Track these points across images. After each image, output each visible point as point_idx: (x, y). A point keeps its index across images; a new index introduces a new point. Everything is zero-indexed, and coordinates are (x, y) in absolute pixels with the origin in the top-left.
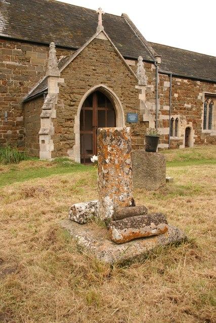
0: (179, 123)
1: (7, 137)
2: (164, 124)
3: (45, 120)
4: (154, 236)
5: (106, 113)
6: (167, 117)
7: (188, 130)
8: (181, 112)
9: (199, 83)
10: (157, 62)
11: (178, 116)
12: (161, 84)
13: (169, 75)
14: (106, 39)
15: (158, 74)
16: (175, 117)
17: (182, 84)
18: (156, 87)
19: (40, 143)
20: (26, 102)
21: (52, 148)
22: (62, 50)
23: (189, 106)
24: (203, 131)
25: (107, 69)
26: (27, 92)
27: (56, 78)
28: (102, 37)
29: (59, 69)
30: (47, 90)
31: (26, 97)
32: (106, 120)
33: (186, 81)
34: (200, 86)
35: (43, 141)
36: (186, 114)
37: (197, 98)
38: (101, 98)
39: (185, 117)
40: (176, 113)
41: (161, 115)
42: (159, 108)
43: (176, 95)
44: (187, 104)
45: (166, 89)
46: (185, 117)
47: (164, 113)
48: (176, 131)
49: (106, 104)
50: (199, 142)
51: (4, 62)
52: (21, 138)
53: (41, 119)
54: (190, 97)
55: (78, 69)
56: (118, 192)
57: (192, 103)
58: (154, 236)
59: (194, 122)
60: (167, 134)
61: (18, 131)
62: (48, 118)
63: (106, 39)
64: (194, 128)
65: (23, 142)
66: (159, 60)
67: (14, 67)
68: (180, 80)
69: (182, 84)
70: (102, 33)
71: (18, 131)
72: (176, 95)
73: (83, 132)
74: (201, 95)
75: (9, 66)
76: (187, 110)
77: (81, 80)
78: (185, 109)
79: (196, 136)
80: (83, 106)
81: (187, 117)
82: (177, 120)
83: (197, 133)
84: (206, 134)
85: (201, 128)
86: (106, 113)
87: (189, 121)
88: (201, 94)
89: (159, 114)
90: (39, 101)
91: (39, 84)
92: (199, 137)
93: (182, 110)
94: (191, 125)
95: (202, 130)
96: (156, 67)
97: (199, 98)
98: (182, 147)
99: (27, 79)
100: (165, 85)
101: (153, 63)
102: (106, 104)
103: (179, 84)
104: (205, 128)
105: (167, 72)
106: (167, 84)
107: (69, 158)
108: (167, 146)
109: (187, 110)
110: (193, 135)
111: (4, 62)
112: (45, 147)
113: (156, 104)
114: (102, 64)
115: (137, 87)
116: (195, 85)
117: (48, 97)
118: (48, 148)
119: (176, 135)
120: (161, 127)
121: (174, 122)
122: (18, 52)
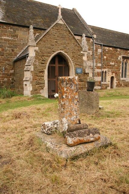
0: (107, 74)
1: (4, 82)
2: (98, 74)
3: (27, 72)
4: (92, 142)
6: (100, 71)
7: (112, 78)
8: (108, 68)
9: (119, 50)
10: (94, 38)
11: (107, 70)
12: (96, 50)
13: (101, 45)
14: (63, 24)
15: (94, 45)
16: (104, 70)
17: (109, 50)
18: (93, 52)
19: (24, 86)
20: (16, 61)
21: (31, 89)
22: (37, 30)
23: (113, 64)
24: (121, 79)
25: (64, 41)
26: (16, 55)
27: (34, 47)
28: (61, 22)
29: (35, 42)
30: (28, 54)
31: (15, 58)
32: (63, 72)
33: (111, 49)
34: (119, 52)
35: (26, 85)
36: (111, 69)
37: (117, 59)
38: (60, 59)
39: (110, 70)
40: (105, 68)
41: (96, 69)
42: (95, 65)
43: (105, 57)
44: (112, 62)
45: (99, 54)
46: (110, 70)
47: (98, 68)
48: (105, 79)
49: (63, 62)
50: (119, 85)
51: (2, 37)
52: (13, 83)
53: (25, 72)
54: (114, 58)
55: (46, 42)
56: (71, 115)
57: (115, 62)
58: (92, 142)
59: (116, 74)
60: (100, 80)
61: (11, 79)
62: (29, 71)
63: (63, 24)
64: (116, 77)
65: (14, 85)
66: (95, 36)
67: (9, 40)
68: (107, 48)
69: (109, 50)
70: (61, 20)
71: (11, 79)
72: (105, 57)
73: (49, 79)
74: (120, 57)
75: (5, 40)
76: (112, 66)
77: (48, 48)
78: (110, 65)
79: (117, 82)
80: (49, 64)
81: (112, 70)
82: (106, 72)
83: (118, 80)
84: (123, 80)
85: (120, 77)
87: (113, 73)
88: (120, 57)
89: (95, 69)
90: (24, 61)
91: (23, 51)
92: (119, 82)
93: (109, 66)
94: (114, 75)
95: (121, 78)
96: (93, 40)
97: (119, 59)
98: (109, 88)
99: (16, 48)
100: (98, 51)
101: (91, 38)
102: (63, 62)
103: (107, 50)
104: (122, 77)
105: (100, 43)
106: (100, 51)
108: (100, 87)
109: (112, 66)
110: (115, 81)
111: (2, 37)
112: (27, 88)
113: (93, 62)
114: (61, 38)
115: (82, 52)
116: (117, 51)
117: (29, 58)
118: (28, 89)
119: (105, 81)
120: (96, 76)
121: (104, 73)
122: (11, 31)
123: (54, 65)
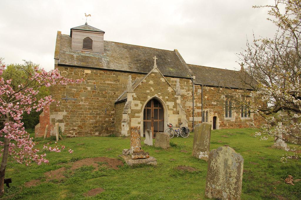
0: (209, 114)
1: (105, 122)
2: (198, 114)
3: (125, 114)
4: (144, 158)
6: (200, 111)
7: (215, 118)
8: (209, 107)
10: (193, 79)
11: (208, 110)
12: (196, 91)
13: (201, 85)
14: (158, 72)
15: (194, 85)
16: (206, 110)
17: (210, 90)
18: (192, 93)
19: (122, 126)
20: (117, 103)
21: (128, 129)
23: (215, 103)
24: (225, 119)
25: (158, 87)
26: (117, 98)
27: (132, 93)
28: (156, 71)
29: (133, 89)
30: (127, 99)
31: (116, 101)
32: (158, 114)
33: (212, 88)
35: (123, 125)
37: (220, 98)
38: (156, 102)
39: (212, 110)
40: (206, 108)
41: (196, 110)
43: (206, 97)
45: (199, 94)
46: (212, 110)
47: (198, 108)
48: (207, 119)
49: (158, 105)
50: (223, 125)
51: (106, 82)
52: (113, 122)
53: (123, 114)
55: (143, 88)
56: (135, 145)
58: (144, 158)
59: (219, 113)
60: (200, 121)
61: (111, 119)
62: (126, 113)
63: (158, 72)
65: (114, 125)
66: (194, 77)
67: (111, 84)
69: (210, 90)
70: (156, 69)
71: (111, 119)
72: (206, 97)
73: (146, 121)
75: (108, 84)
76: (214, 106)
77: (144, 94)
78: (212, 105)
79: (221, 122)
80: (145, 107)
81: (214, 110)
82: (207, 112)
83: (221, 120)
84: (227, 120)
85: (224, 117)
90: (123, 104)
91: (124, 93)
92: (223, 122)
95: (225, 118)
96: (193, 81)
99: (117, 91)
100: (198, 92)
101: (191, 79)
102: (158, 105)
103: (208, 90)
104: (226, 116)
105: (200, 84)
106: (200, 91)
109: (214, 106)
110: (218, 121)
111: (106, 82)
112: (124, 129)
113: (193, 102)
114: (156, 85)
115: (175, 96)
117: (127, 102)
118: (126, 128)
119: (207, 121)
120: (196, 116)
121: (205, 114)
122: (113, 77)
123: (51, 120)
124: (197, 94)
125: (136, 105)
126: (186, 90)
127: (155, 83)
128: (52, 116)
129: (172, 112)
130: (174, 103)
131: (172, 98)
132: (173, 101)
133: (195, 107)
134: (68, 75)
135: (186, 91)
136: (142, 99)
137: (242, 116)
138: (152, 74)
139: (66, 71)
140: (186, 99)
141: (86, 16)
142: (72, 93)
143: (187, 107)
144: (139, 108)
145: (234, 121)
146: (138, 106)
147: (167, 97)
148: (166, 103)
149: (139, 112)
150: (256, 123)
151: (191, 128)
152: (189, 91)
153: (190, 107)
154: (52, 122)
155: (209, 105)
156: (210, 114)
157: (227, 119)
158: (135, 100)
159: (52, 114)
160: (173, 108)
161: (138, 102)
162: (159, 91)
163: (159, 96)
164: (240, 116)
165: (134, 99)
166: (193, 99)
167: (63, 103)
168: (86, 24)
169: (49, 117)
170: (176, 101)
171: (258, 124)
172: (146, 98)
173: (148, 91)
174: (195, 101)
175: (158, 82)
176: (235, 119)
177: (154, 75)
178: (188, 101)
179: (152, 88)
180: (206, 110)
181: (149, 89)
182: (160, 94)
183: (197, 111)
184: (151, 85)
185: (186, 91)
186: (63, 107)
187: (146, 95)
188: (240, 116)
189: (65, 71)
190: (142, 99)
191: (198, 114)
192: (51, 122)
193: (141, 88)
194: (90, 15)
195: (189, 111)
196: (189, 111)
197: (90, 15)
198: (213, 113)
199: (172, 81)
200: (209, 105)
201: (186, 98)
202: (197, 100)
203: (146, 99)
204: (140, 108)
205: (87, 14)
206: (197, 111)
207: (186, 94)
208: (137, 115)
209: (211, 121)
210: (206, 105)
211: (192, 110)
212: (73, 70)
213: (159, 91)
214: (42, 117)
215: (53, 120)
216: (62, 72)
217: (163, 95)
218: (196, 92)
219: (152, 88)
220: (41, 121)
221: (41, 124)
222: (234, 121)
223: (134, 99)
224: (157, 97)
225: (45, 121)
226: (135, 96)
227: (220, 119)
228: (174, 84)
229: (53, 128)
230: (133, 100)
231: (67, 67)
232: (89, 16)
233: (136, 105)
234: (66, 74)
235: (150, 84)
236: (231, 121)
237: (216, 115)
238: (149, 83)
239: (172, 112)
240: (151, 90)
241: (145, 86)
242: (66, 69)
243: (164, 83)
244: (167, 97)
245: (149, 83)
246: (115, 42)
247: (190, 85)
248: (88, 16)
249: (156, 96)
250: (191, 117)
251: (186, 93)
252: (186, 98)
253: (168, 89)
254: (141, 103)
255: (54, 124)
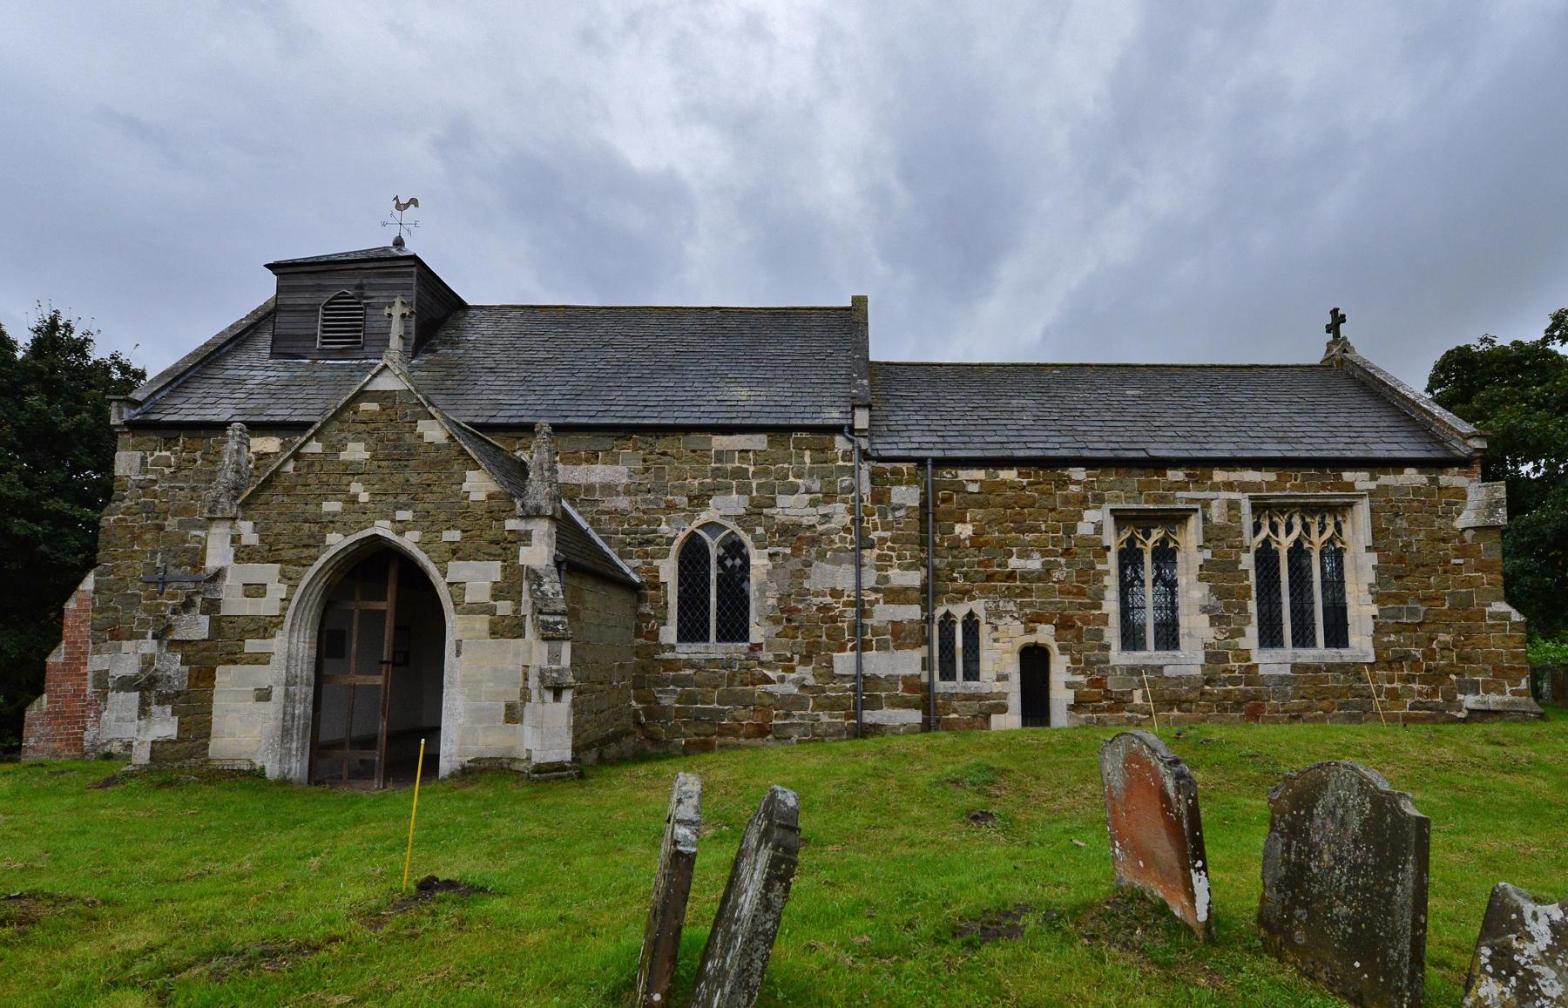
0: (984, 631)
5: (356, 618)
7: (1034, 662)
9: (1078, 474)
11: (979, 607)
12: (880, 497)
16: (960, 611)
22: (517, 434)
23: (1035, 564)
25: (399, 478)
34: (1087, 486)
36: (1017, 596)
39: (1011, 606)
40: (964, 594)
42: (870, 578)
43: (964, 530)
44: (1019, 557)
47: (897, 596)
54: (1036, 529)
57: (1044, 554)
59: (1064, 625)
64: (1063, 650)
68: (980, 474)
69: (989, 488)
72: (964, 530)
74: (1095, 521)
76: (1023, 578)
77: (306, 521)
78: (1011, 576)
79: (1080, 678)
81: (1021, 606)
82: (971, 623)
83: (1090, 664)
84: (1134, 670)
85: (1107, 648)
86: (356, 618)
87: (1031, 622)
88: (1091, 515)
89: (872, 603)
93: (996, 580)
94: (1045, 634)
97: (1084, 528)
98: (1009, 721)
100: (895, 500)
103: (974, 488)
107: (762, 847)
108: (915, 717)
110: (1060, 671)
114: (383, 464)
115: (511, 524)
116: (1064, 483)
119: (972, 673)
120: (883, 646)
123: (90, 676)
124: (883, 515)
125: (255, 590)
126: (807, 497)
127: (381, 453)
128: (96, 663)
129: (482, 623)
130: (504, 569)
131: (489, 535)
132: (492, 557)
133: (875, 590)
134: (179, 468)
135: (814, 503)
136: (289, 554)
137: (1270, 637)
138: (364, 406)
139: (168, 453)
140: (813, 551)
141: (399, 206)
142: (186, 551)
143: (817, 594)
144: (267, 606)
145: (1196, 671)
146: (263, 595)
147: (454, 535)
148: (444, 575)
149: (265, 627)
150: (1397, 685)
151: (848, 717)
152: (829, 497)
153: (836, 594)
154: (95, 687)
155: (990, 578)
156: (996, 629)
157: (1132, 662)
158: (250, 560)
159: (98, 652)
160: (495, 597)
161: (267, 573)
162: (403, 499)
163: (401, 533)
164: (1243, 643)
165: (244, 554)
166: (864, 542)
167: (146, 599)
168: (399, 243)
169: (86, 664)
170: (517, 556)
171: (1420, 694)
172: (318, 542)
173: (332, 506)
174: (870, 555)
175: (395, 447)
176: (1201, 658)
177: (374, 407)
178: (821, 556)
179: (356, 487)
180: (960, 611)
181: (338, 491)
182: (402, 515)
183: (884, 613)
184: (353, 470)
185: (814, 503)
186: (143, 616)
187: (315, 528)
188: (1243, 643)
189: (164, 453)
190: (289, 554)
191: (900, 636)
192: (89, 689)
193: (288, 492)
194: (414, 202)
195: (834, 620)
196: (834, 620)
197: (414, 202)
198: (1018, 627)
199: (720, 456)
200: (990, 578)
201: (814, 541)
202: (889, 548)
203: (313, 551)
204: (278, 604)
205: (403, 201)
206: (884, 613)
207: (814, 520)
208: (252, 646)
209: (1002, 678)
210: (965, 576)
211: (851, 613)
212: (197, 443)
213: (403, 499)
214: (56, 664)
215: (101, 678)
216: (149, 460)
217: (428, 523)
218: (881, 502)
219: (356, 487)
220: (50, 684)
221: (49, 697)
222: (1196, 671)
223: (244, 554)
224: (389, 535)
225: (68, 686)
226: (249, 536)
227: (1074, 661)
228: (729, 466)
229: (99, 713)
230: (237, 559)
231: (173, 434)
232: (412, 206)
233: (255, 590)
234: (170, 466)
235: (348, 464)
236: (1168, 671)
237: (1045, 634)
238: (343, 456)
239: (482, 623)
240: (354, 499)
241: (312, 479)
242: (169, 443)
243: (438, 448)
244: (454, 535)
245: (343, 456)
246: (522, 307)
247: (840, 463)
248: (407, 206)
249: (383, 529)
250: (848, 653)
251: (809, 516)
252: (814, 541)
253: (466, 486)
254: (284, 576)
255: (104, 698)
